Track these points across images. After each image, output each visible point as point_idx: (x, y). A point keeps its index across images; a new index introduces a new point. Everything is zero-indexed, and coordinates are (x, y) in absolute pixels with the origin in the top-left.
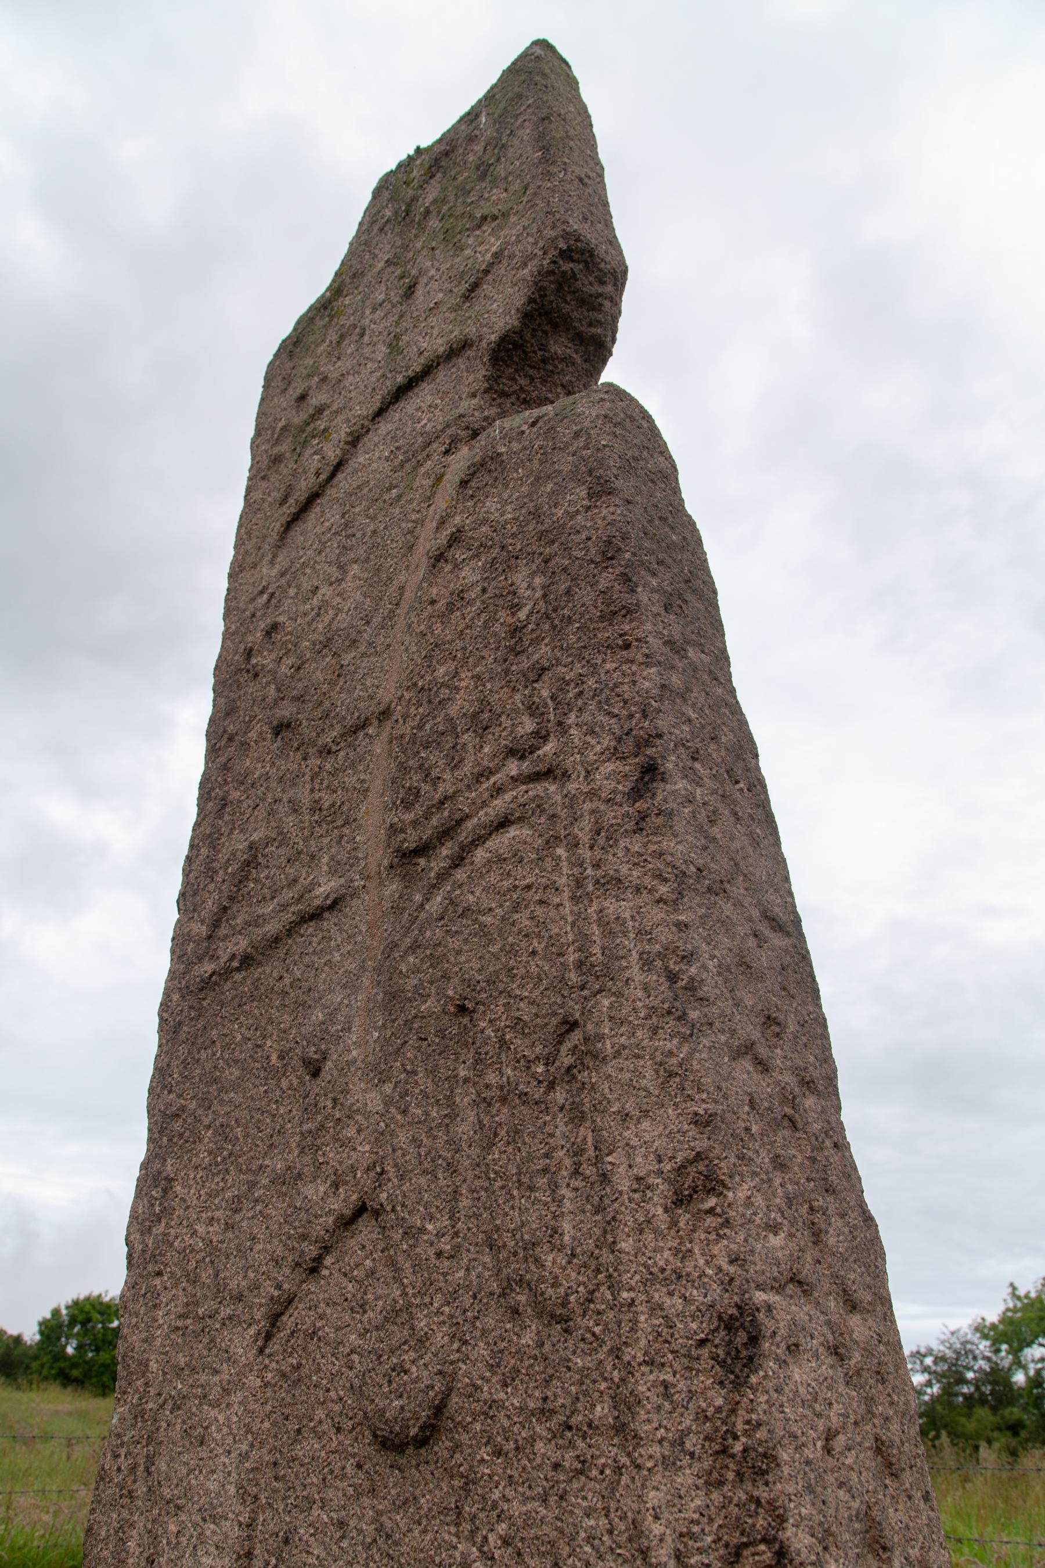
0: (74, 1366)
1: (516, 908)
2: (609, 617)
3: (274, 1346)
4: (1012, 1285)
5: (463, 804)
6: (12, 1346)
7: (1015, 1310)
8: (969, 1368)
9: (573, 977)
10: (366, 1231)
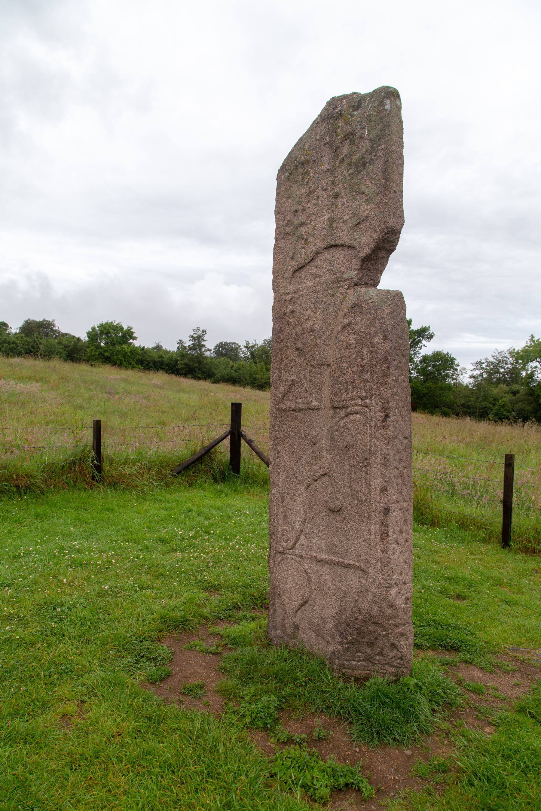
0: (106, 351)
1: (359, 433)
2: (383, 377)
3: (308, 490)
4: (532, 335)
5: (349, 403)
6: (76, 342)
7: (530, 347)
8: (502, 367)
9: (368, 451)
10: (326, 478)
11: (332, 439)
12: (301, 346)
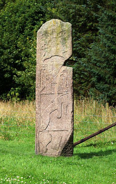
11: (58, 101)
12: (48, 78)
